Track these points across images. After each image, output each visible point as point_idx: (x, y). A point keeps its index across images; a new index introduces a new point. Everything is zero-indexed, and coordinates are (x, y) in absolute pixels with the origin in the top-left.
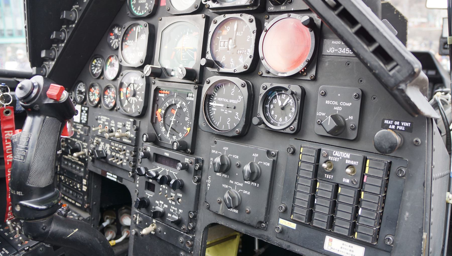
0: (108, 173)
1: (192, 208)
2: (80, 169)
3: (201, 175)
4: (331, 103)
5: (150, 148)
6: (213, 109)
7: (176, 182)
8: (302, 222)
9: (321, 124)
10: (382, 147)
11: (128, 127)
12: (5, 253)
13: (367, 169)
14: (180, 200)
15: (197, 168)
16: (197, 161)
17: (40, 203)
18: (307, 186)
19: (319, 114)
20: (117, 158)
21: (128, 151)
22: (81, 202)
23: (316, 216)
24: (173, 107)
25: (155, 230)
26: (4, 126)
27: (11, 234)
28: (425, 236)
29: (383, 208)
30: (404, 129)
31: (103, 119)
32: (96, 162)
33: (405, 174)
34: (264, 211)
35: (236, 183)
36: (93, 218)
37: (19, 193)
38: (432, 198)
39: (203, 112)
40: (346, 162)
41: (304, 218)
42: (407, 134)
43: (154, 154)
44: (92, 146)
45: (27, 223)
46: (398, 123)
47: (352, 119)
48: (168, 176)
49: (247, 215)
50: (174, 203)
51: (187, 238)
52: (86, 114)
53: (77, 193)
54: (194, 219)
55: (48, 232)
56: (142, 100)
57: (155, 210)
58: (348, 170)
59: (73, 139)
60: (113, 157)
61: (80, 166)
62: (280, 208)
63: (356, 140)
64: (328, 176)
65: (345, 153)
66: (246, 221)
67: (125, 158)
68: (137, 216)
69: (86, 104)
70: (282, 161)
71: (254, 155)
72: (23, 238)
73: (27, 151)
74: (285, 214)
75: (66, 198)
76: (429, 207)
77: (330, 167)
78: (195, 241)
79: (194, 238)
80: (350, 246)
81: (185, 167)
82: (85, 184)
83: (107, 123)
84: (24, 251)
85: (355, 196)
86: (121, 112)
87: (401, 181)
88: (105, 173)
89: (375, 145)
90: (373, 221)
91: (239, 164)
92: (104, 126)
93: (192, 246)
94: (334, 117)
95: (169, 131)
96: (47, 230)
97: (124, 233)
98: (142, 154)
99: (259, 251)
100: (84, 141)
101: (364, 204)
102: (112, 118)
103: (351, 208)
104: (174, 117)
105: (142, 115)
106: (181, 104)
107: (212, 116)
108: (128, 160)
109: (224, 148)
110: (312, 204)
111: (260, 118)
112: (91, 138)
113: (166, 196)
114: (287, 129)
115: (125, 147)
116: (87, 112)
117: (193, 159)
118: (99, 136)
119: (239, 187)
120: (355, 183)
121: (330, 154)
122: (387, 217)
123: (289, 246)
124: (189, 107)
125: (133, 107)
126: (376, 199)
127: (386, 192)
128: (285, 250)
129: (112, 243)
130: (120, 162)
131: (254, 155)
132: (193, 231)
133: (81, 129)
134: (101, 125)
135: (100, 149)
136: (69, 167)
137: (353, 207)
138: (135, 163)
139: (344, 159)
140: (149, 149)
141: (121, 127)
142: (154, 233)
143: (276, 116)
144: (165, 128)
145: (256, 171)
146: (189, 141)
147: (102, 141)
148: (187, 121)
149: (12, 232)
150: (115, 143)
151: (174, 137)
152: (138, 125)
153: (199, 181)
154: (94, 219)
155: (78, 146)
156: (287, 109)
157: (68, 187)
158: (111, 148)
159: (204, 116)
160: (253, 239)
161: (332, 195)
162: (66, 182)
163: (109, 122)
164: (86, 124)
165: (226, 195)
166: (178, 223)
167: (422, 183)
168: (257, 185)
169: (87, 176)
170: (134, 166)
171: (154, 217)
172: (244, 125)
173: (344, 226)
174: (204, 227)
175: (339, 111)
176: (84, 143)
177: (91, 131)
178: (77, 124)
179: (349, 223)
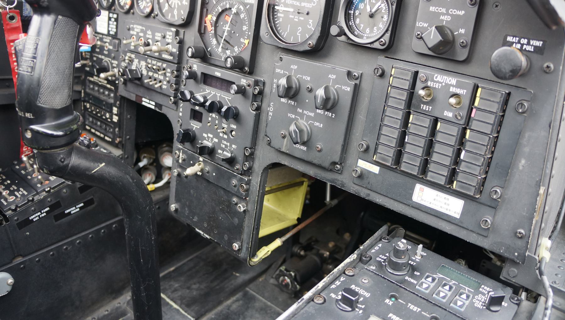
0: (144, 99)
1: (248, 144)
2: (109, 95)
3: (262, 101)
4: (437, 10)
5: (197, 66)
6: (279, 15)
7: (229, 109)
8: (388, 164)
9: (421, 38)
10: (500, 71)
11: (170, 34)
12: (23, 194)
13: (477, 100)
14: (233, 133)
15: (256, 92)
16: (257, 83)
17: (57, 128)
18: (396, 119)
19: (419, 24)
20: (155, 80)
21: (169, 70)
22: (111, 135)
23: (405, 158)
24: (227, 13)
25: (202, 170)
26: (9, 36)
27: (29, 172)
28: (542, 191)
29: (493, 153)
30: (532, 50)
31: (137, 29)
32: (129, 85)
33: (527, 110)
34: (339, 148)
35: (305, 112)
36: (126, 156)
37: (28, 115)
38: (558, 143)
39: (266, 19)
40: (451, 90)
41: (391, 159)
42: (535, 57)
43: (202, 73)
44: (123, 64)
45: (41, 153)
46: (525, 41)
47: (463, 33)
48: (219, 102)
49: (318, 153)
50: (225, 137)
51: (241, 180)
52: (115, 23)
53: (106, 125)
54: (251, 157)
55: (67, 165)
56: (187, 3)
57: (202, 145)
58: (453, 101)
59: (100, 56)
60: (150, 78)
61: (110, 90)
62: (361, 145)
63: (466, 61)
64: (425, 107)
65: (450, 78)
66: (315, 161)
67: (165, 79)
68: (180, 152)
69: (115, 10)
70: (366, 86)
71: (330, 76)
72: (43, 178)
73: (35, 60)
74: (366, 153)
75: (93, 131)
76: (553, 155)
77: (429, 95)
78: (251, 184)
79: (249, 181)
80: (445, 198)
81: (241, 91)
82: (116, 112)
83: (142, 34)
84: (44, 193)
85: (458, 134)
86: (160, 19)
87: (520, 118)
88: (140, 98)
89: (491, 68)
90: (479, 168)
91: (310, 87)
92: (139, 38)
93: (247, 190)
94: (440, 29)
95: (221, 44)
96: (65, 163)
97: (165, 176)
98: (186, 73)
99: (330, 203)
100: (114, 58)
101: (468, 146)
102: (148, 28)
103: (452, 149)
104: (228, 25)
105: (187, 23)
106: (238, 8)
107: (277, 24)
108: (168, 82)
109: (292, 67)
110: (402, 142)
111: (341, 28)
112: (121, 54)
113: (216, 127)
114: (375, 44)
115: (165, 66)
116: (116, 20)
117: (251, 80)
118: (132, 52)
119: (309, 118)
120: (459, 118)
121: (430, 79)
122: (497, 163)
123: (369, 195)
124: (249, 12)
125: (175, 12)
126: (485, 140)
127: (498, 132)
128: (364, 199)
129: (151, 187)
130: (159, 85)
131: (330, 77)
132: (248, 172)
133: (104, 50)
134: (134, 37)
135: (134, 67)
136: (95, 91)
137: (454, 149)
138: (177, 86)
139: (448, 86)
140: (195, 68)
141: (159, 39)
142: (201, 174)
143: (362, 25)
144: (217, 40)
145: (332, 97)
146: (247, 57)
147: (136, 58)
148: (246, 31)
149: (30, 170)
150: (152, 60)
151: (228, 52)
152: (182, 36)
153: (258, 109)
154: (127, 158)
155: (106, 64)
156: (378, 17)
157: (95, 117)
158: (147, 67)
159: (267, 24)
160: (325, 184)
161: (428, 132)
162: (92, 111)
163: (145, 33)
164: (115, 37)
165: (293, 128)
166: (231, 161)
167: (548, 123)
168: (332, 115)
169: (118, 102)
170: (177, 90)
171: (201, 154)
172: (319, 37)
173: (440, 173)
174: (263, 168)
175: (447, 21)
176: (113, 62)
177: (122, 45)
178: (104, 36)
179: (447, 169)
